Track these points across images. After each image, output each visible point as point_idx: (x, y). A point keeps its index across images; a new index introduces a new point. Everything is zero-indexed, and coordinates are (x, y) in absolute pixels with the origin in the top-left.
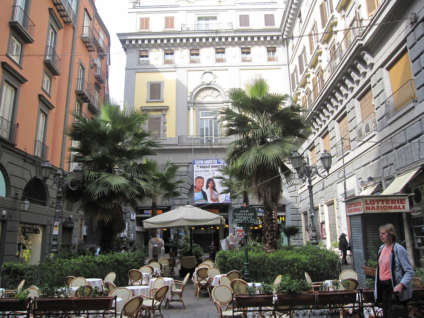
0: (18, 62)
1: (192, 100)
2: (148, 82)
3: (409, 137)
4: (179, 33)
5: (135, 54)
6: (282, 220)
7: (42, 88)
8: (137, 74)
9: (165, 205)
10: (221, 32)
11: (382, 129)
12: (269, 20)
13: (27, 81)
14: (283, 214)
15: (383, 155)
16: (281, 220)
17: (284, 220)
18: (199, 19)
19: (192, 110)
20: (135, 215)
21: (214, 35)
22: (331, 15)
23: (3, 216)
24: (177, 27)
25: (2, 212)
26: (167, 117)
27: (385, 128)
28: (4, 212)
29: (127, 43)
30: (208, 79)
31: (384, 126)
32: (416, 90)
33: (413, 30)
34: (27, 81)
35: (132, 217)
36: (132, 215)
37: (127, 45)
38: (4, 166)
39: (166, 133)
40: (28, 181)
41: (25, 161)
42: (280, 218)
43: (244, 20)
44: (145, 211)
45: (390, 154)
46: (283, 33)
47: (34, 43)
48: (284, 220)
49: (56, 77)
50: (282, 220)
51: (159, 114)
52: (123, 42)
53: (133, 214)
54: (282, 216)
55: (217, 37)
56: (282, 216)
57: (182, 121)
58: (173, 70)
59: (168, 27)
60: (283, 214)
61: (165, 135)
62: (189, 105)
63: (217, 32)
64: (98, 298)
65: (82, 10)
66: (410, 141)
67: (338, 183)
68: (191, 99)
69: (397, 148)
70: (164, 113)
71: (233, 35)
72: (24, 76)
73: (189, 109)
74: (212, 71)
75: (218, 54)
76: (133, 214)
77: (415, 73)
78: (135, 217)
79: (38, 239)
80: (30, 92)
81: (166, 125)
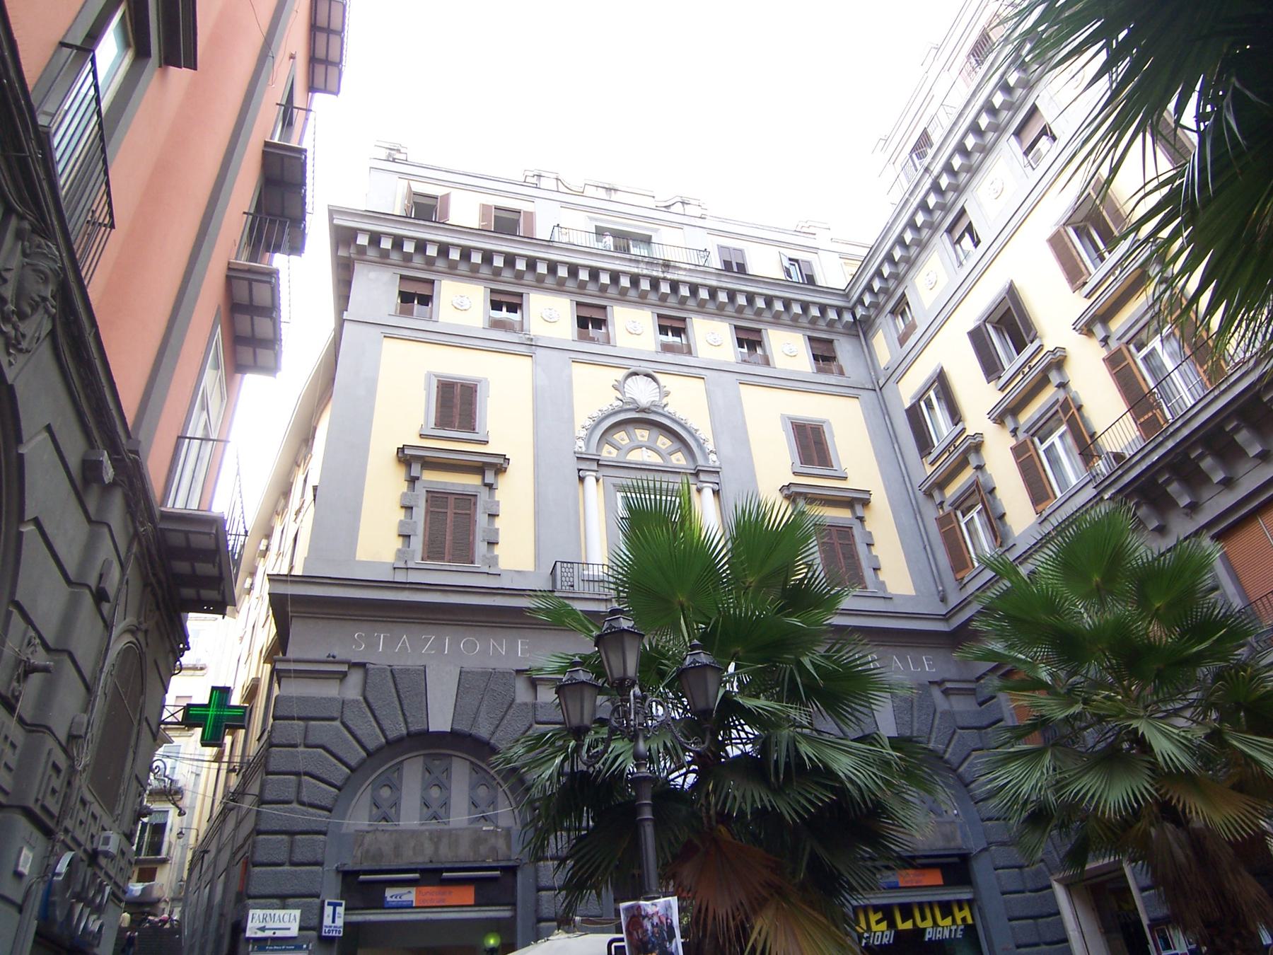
1: (593, 450)
2: (429, 375)
6: (964, 919)
8: (387, 342)
9: (490, 862)
10: (679, 268)
13: (194, 67)
14: (965, 894)
16: (959, 922)
17: (970, 921)
19: (590, 480)
20: (340, 910)
21: (657, 273)
26: (499, 495)
30: (642, 392)
34: (194, 67)
35: (327, 921)
36: (328, 910)
39: (497, 550)
42: (956, 910)
44: (390, 893)
48: (970, 921)
50: (964, 919)
51: (469, 482)
53: (335, 905)
54: (960, 904)
55: (665, 279)
56: (960, 904)
57: (553, 516)
58: (523, 349)
60: (965, 894)
61: (494, 561)
62: (583, 465)
63: (667, 265)
68: (587, 445)
70: (489, 478)
73: (581, 479)
74: (657, 375)
76: (335, 905)
78: (340, 922)
79: (800, 312)
81: (498, 523)
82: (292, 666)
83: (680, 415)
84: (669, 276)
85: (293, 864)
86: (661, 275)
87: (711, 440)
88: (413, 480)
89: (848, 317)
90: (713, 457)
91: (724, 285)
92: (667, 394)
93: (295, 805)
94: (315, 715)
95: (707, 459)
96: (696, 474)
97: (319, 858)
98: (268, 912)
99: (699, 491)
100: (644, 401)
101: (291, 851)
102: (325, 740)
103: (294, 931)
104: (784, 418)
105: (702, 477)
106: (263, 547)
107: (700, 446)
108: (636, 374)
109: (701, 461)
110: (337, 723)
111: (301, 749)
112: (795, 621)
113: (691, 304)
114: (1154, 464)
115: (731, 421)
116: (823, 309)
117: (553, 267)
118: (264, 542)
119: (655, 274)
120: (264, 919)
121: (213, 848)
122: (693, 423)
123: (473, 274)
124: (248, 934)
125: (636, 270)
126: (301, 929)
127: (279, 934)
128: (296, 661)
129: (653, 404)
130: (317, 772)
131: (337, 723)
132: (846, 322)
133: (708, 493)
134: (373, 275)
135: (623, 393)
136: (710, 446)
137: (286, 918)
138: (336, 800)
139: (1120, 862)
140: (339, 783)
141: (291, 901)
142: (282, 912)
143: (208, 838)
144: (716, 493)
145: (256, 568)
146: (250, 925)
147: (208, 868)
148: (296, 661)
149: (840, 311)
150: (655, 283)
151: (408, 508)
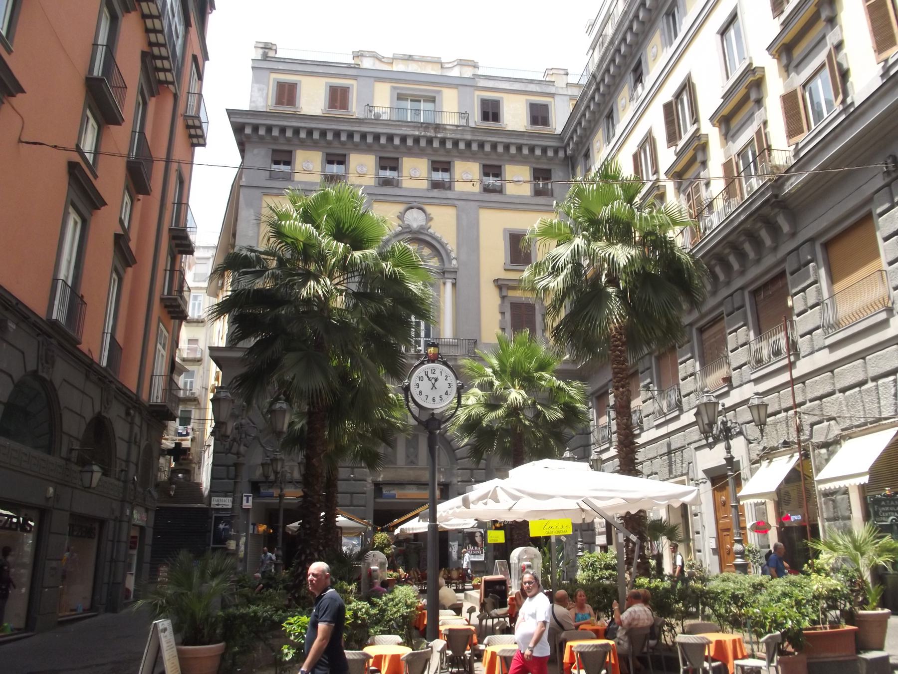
0: (91, 162)
2: (505, 230)
3: (873, 372)
4: (360, 121)
5: (260, 156)
7: (121, 219)
11: (812, 353)
12: (539, 115)
15: (811, 401)
18: (401, 97)
20: (251, 499)
21: (431, 133)
22: (691, 129)
23: (47, 499)
24: (356, 109)
25: (47, 490)
27: (818, 351)
28: (51, 490)
29: (248, 131)
30: (415, 219)
31: (817, 348)
32: (892, 290)
33: (888, 185)
36: (245, 498)
37: (248, 137)
38: (57, 387)
40: (88, 420)
41: (87, 377)
43: (491, 111)
45: (828, 399)
46: (568, 144)
47: (123, 124)
49: (141, 197)
52: (238, 129)
59: (335, 107)
64: (809, 629)
65: (189, 59)
66: (875, 379)
67: (697, 449)
69: (843, 390)
71: (469, 137)
72: (102, 194)
75: (436, 173)
77: (890, 259)
80: (106, 224)
83: (438, 235)
84: (439, 135)
86: (433, 135)
87: (455, 251)
88: (503, 298)
89: (561, 154)
90: (454, 262)
91: (476, 138)
92: (431, 219)
95: (451, 263)
96: (444, 273)
99: (444, 284)
100: (415, 225)
104: (505, 230)
105: (446, 276)
107: (448, 254)
108: (412, 208)
109: (447, 265)
112: (12, 326)
113: (296, 141)
115: (469, 234)
116: (544, 150)
117: (364, 136)
119: (428, 134)
122: (445, 240)
123: (368, 149)
125: (417, 133)
129: (422, 227)
132: (557, 156)
133: (449, 285)
134: (256, 151)
135: (403, 221)
136: (453, 255)
139: (213, 491)
144: (454, 285)
149: (556, 151)
150: (430, 141)
151: (503, 313)
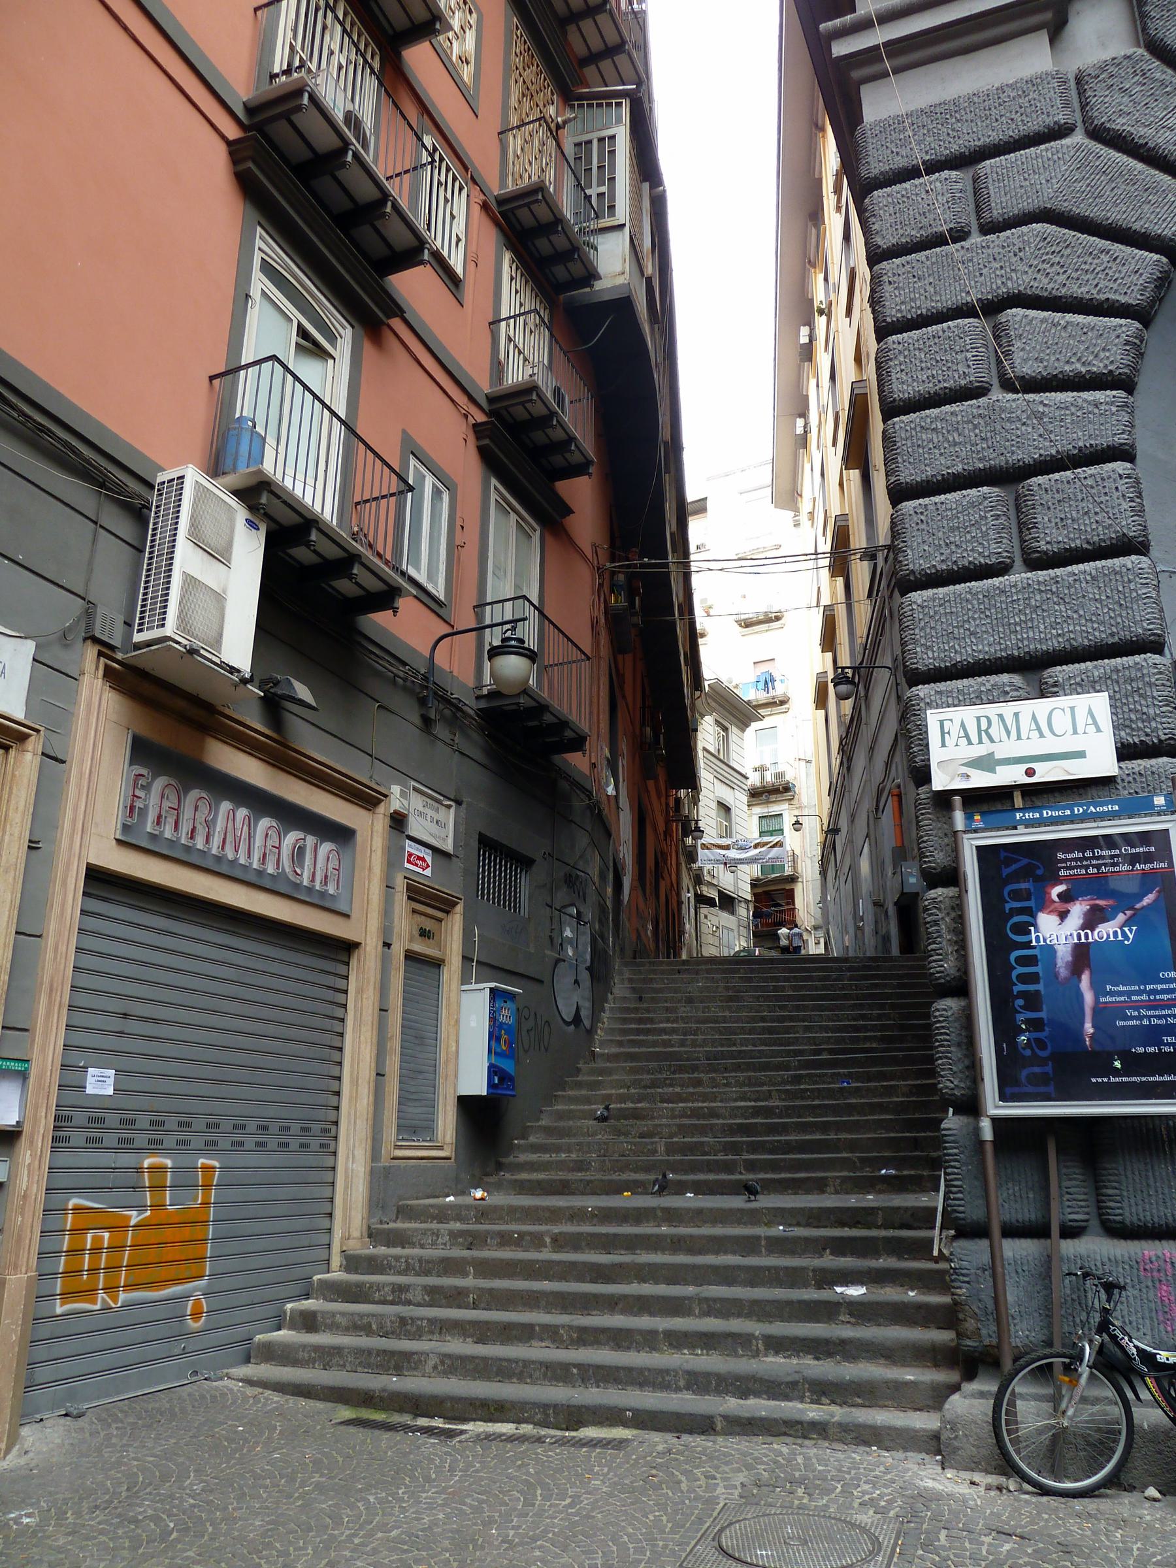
82: (879, 36)
85: (1038, 561)
93: (997, 394)
94: (992, 136)
97: (1128, 526)
98: (992, 710)
101: (1024, 526)
102: (1046, 196)
103: (1101, 761)
106: (804, 340)
110: (1079, 138)
111: (976, 239)
114: (700, 1189)
118: (804, 331)
120: (984, 733)
121: (844, 824)
124: (940, 781)
126: (1125, 752)
127: (1046, 773)
128: (889, 17)
130: (1043, 285)
131: (1079, 138)
137: (1062, 722)
138: (1137, 349)
140: (1132, 298)
141: (1060, 672)
142: (1042, 706)
143: (835, 814)
145: (805, 399)
146: (936, 755)
147: (843, 856)
148: (889, 17)
